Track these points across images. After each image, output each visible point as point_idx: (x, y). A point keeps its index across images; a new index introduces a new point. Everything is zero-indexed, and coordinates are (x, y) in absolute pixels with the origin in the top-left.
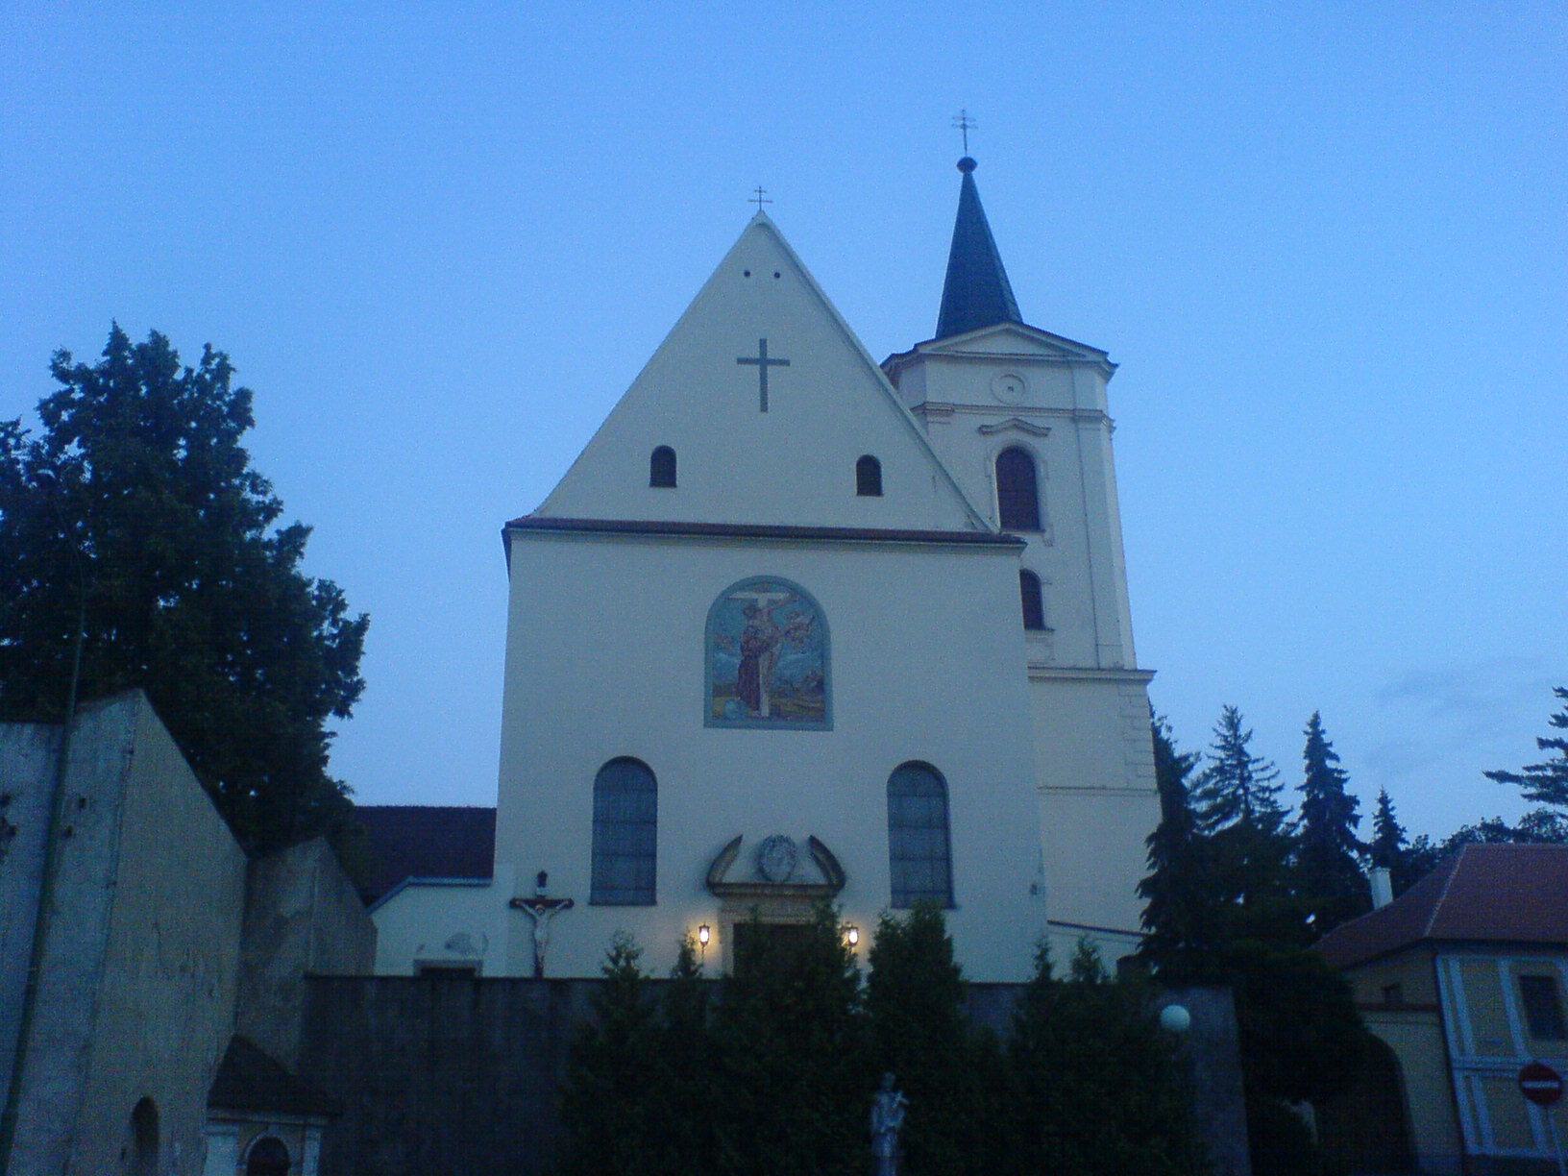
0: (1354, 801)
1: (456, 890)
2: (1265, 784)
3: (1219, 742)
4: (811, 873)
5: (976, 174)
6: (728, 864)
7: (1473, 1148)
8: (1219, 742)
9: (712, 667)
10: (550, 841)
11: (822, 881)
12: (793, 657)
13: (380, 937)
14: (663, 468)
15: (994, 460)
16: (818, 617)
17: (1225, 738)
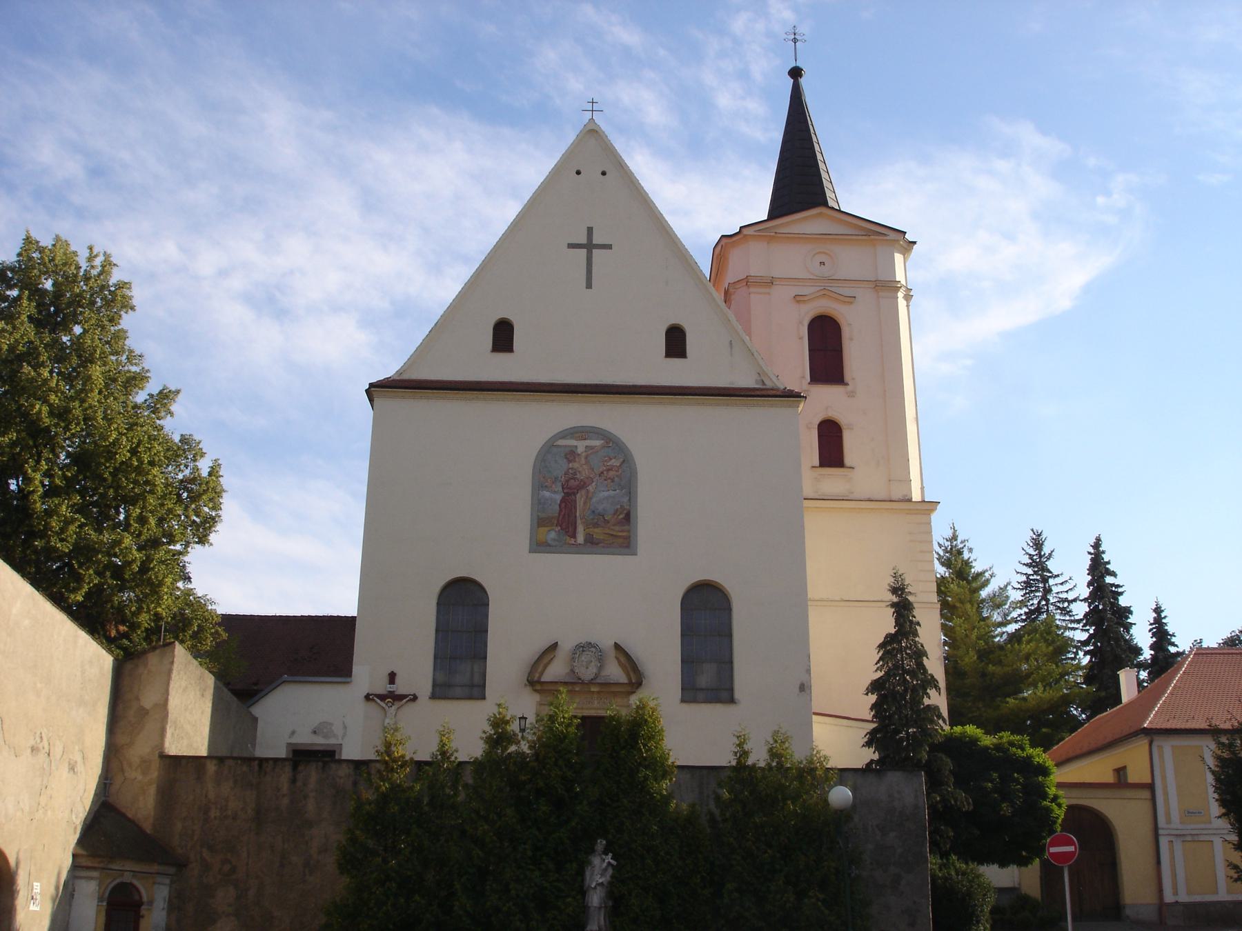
0: (1128, 611)
1: (335, 686)
2: (1064, 596)
3: (1027, 560)
4: (614, 672)
5: (802, 81)
6: (545, 667)
7: (1169, 897)
8: (1027, 560)
9: (538, 503)
10: (404, 647)
11: (624, 679)
12: (606, 494)
13: (260, 724)
14: (503, 336)
15: (806, 323)
16: (627, 460)
17: (1031, 556)
